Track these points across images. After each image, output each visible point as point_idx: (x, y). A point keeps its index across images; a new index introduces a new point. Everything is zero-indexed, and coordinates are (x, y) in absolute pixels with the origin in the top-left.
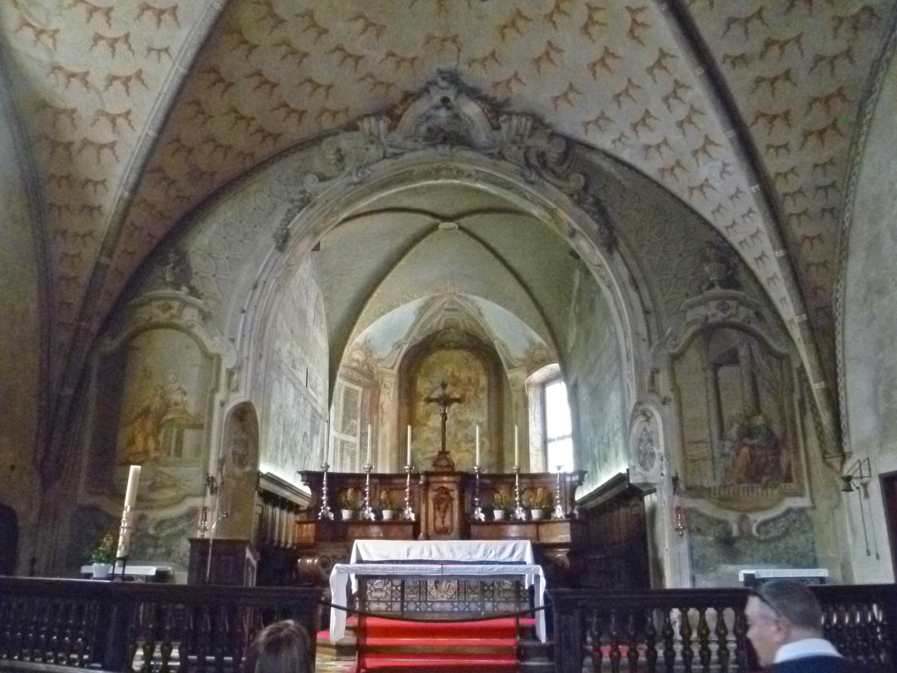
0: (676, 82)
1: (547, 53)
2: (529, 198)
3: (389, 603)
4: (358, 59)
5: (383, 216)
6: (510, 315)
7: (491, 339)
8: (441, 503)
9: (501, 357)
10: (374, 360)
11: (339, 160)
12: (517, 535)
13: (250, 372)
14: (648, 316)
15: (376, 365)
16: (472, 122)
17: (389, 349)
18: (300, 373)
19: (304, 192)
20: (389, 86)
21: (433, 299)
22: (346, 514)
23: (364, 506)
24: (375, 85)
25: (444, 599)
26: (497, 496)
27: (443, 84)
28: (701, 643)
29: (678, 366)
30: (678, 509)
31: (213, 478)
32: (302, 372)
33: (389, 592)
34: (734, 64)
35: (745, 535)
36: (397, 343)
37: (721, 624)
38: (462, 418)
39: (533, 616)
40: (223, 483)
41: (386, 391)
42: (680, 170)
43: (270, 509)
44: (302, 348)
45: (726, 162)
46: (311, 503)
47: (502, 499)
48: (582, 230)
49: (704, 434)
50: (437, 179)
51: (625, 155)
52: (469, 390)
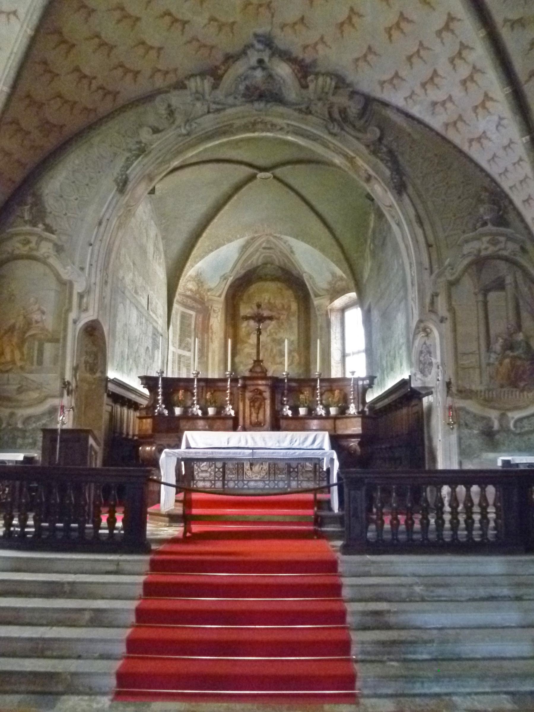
0: (461, 44)
1: (350, 18)
2: (333, 148)
3: (213, 482)
4: (185, 23)
5: (210, 165)
6: (317, 253)
7: (301, 272)
8: (256, 402)
9: (309, 287)
10: (205, 290)
11: (169, 114)
12: (318, 428)
13: (97, 295)
14: (430, 248)
15: (207, 293)
16: (284, 81)
17: (217, 280)
18: (141, 298)
19: (140, 142)
20: (212, 47)
21: (253, 239)
22: (178, 411)
23: (193, 404)
24: (200, 47)
25: (258, 478)
26: (302, 396)
27: (259, 46)
28: (466, 513)
29: (453, 289)
30: (450, 408)
31: (69, 383)
32: (143, 298)
33: (213, 473)
34: (512, 27)
35: (504, 429)
36: (224, 275)
37: (483, 497)
38: (277, 337)
39: (329, 492)
40: (77, 387)
41: (215, 315)
42: (462, 123)
43: (119, 409)
44: (144, 279)
45: (502, 116)
46: (150, 402)
47: (306, 399)
48: (376, 176)
49: (473, 347)
50: (254, 132)
51: (415, 111)
52: (282, 314)
